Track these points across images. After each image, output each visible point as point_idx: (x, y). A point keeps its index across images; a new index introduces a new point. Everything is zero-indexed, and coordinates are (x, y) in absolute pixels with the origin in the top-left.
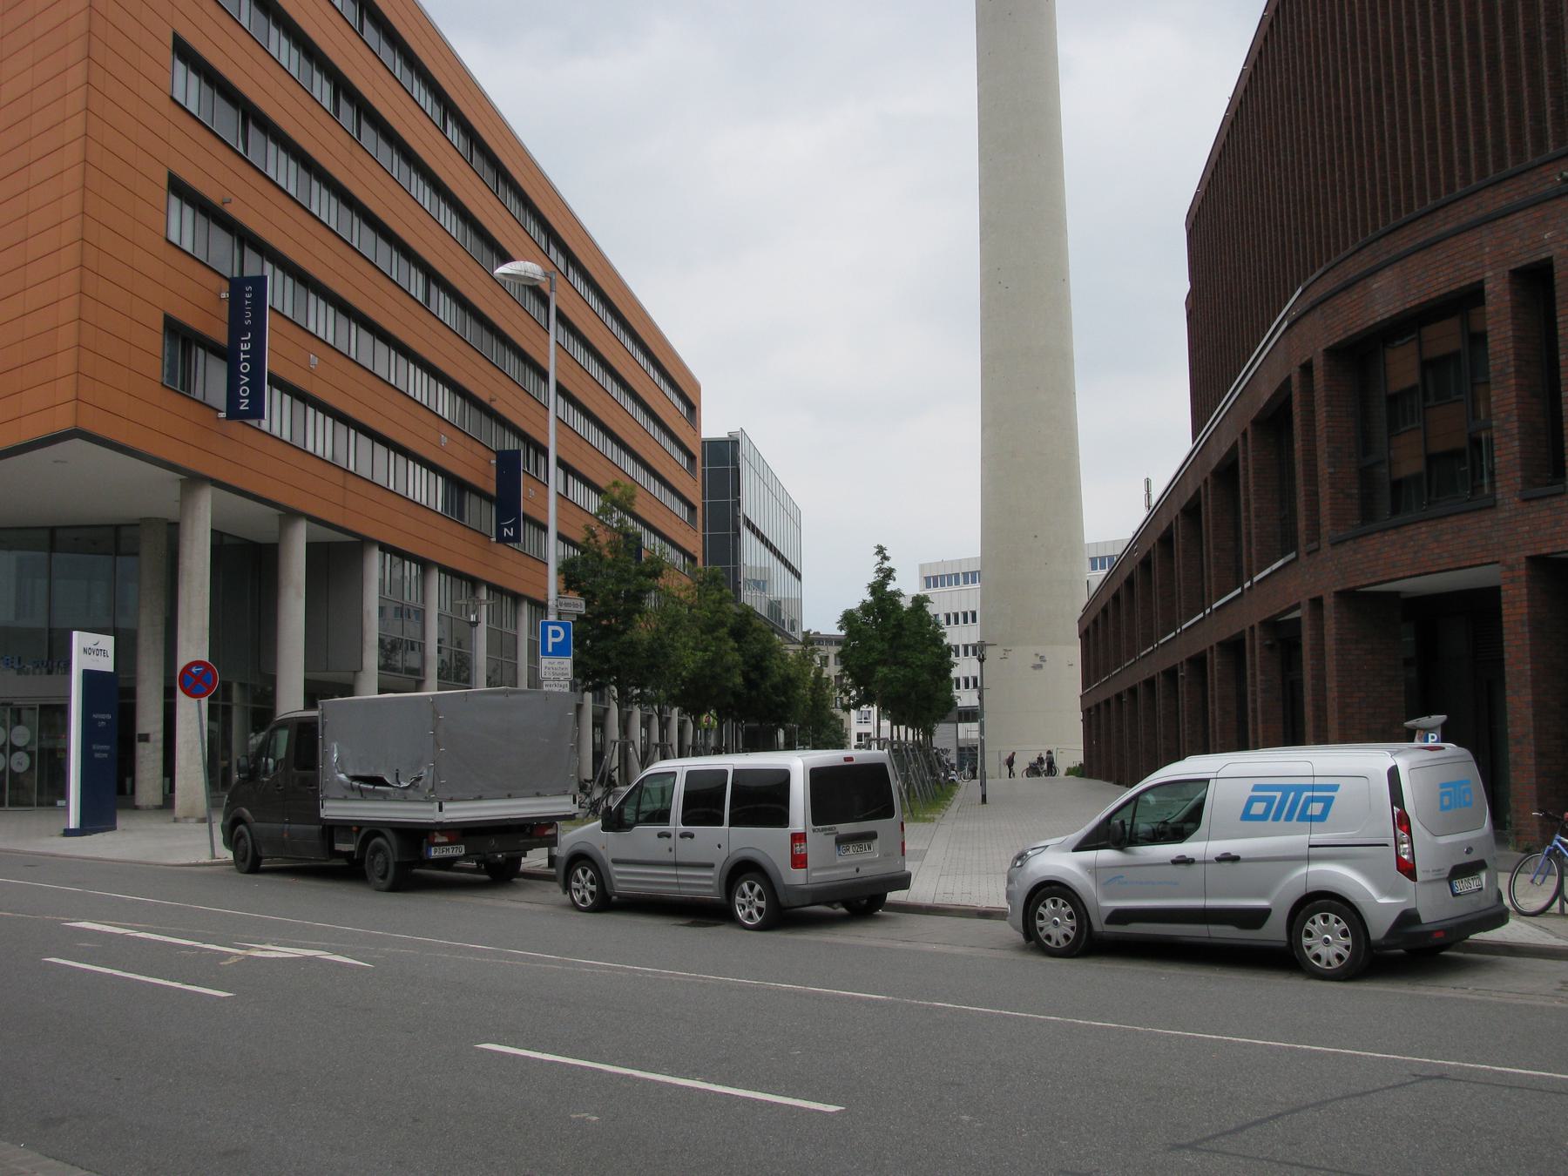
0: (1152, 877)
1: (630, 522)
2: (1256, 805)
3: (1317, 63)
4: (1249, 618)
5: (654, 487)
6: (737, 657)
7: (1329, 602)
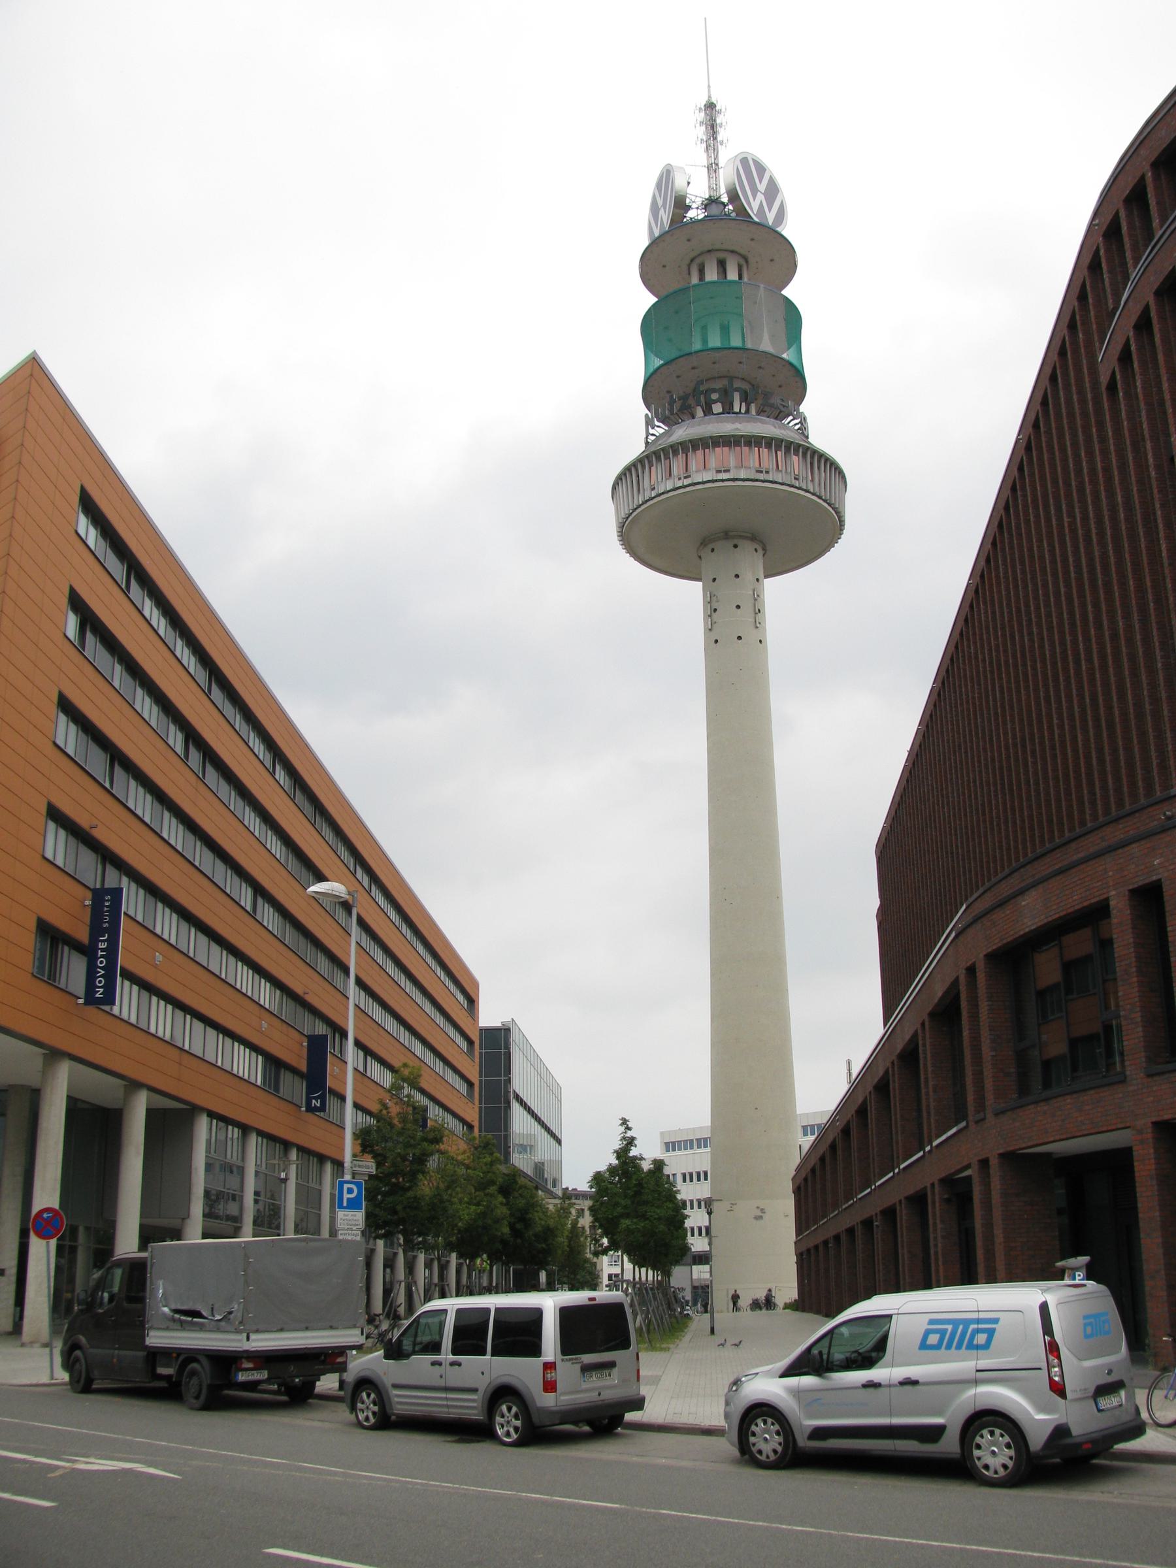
0: (843, 1401)
1: (418, 1096)
2: (931, 1336)
3: (976, 724)
4: (929, 1177)
5: (439, 1067)
6: (505, 1210)
7: (994, 1162)
